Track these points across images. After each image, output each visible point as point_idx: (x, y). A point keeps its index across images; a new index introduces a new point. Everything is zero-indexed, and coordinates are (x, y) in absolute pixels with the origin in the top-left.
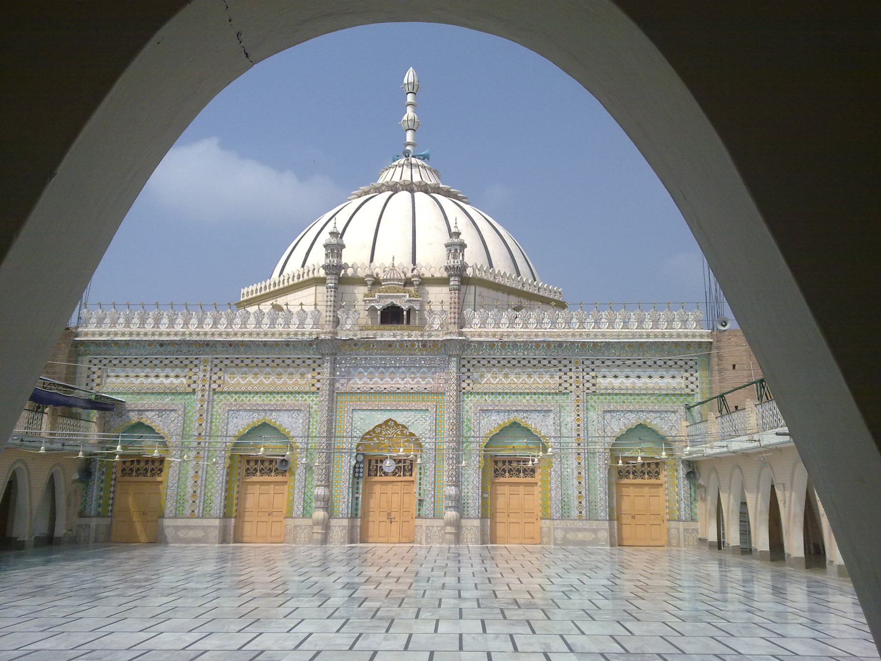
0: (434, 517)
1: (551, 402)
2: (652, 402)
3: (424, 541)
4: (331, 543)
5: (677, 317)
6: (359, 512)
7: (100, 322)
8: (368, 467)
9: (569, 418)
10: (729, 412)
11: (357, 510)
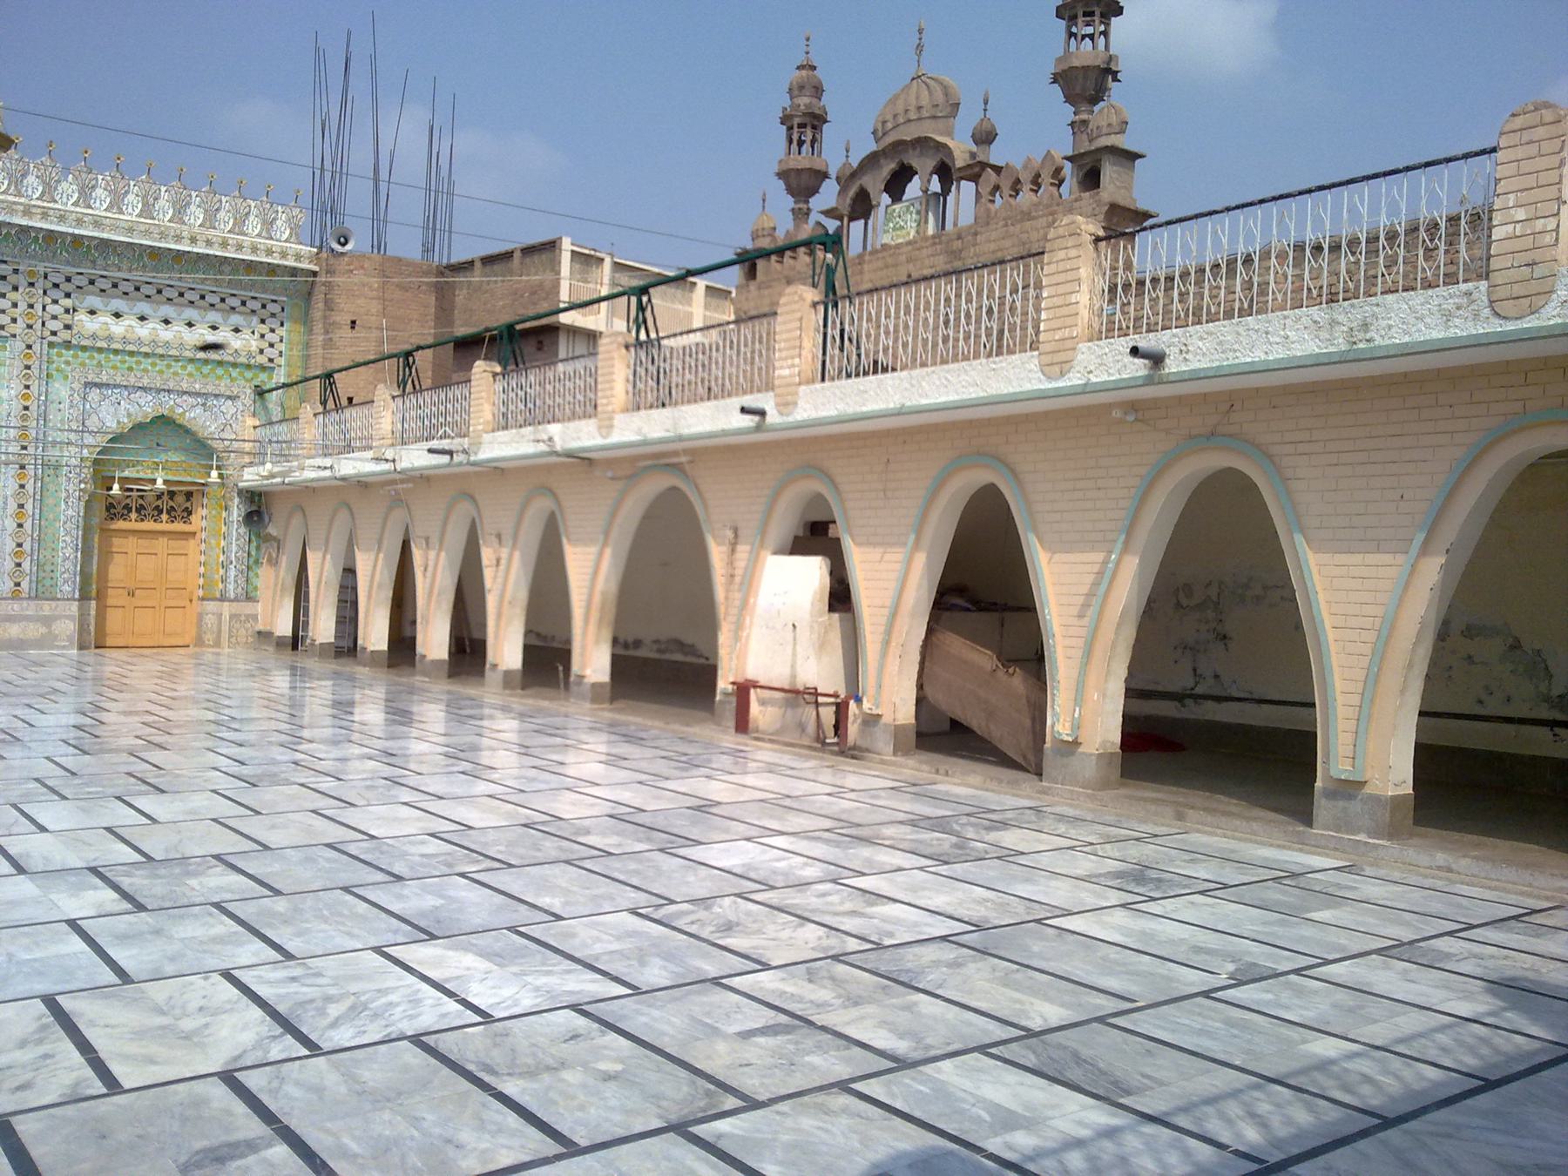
2: (190, 375)
5: (254, 211)
10: (338, 408)
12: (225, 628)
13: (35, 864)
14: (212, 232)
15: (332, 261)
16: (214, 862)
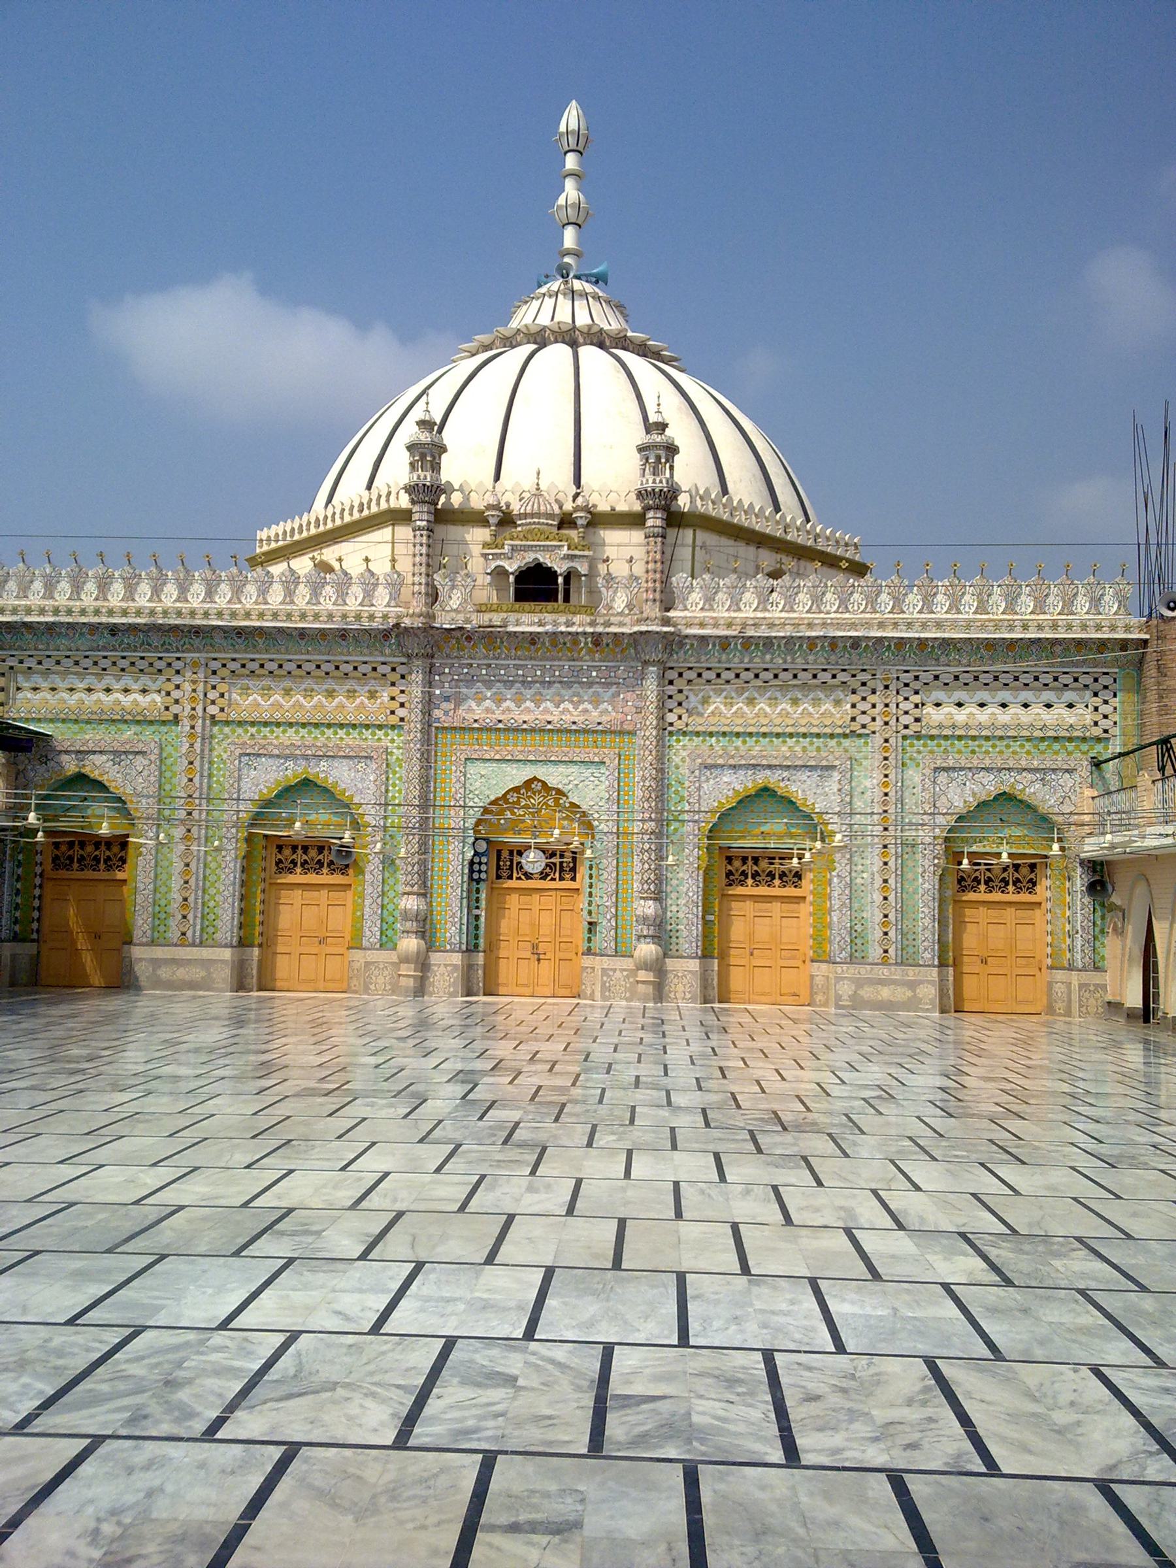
0: (617, 953)
1: (833, 752)
2: (1028, 753)
3: (598, 994)
8: (494, 864)
9: (869, 781)
11: (477, 937)
12: (1075, 997)
13: (911, 1222)
14: (1042, 617)
16: (1077, 1245)
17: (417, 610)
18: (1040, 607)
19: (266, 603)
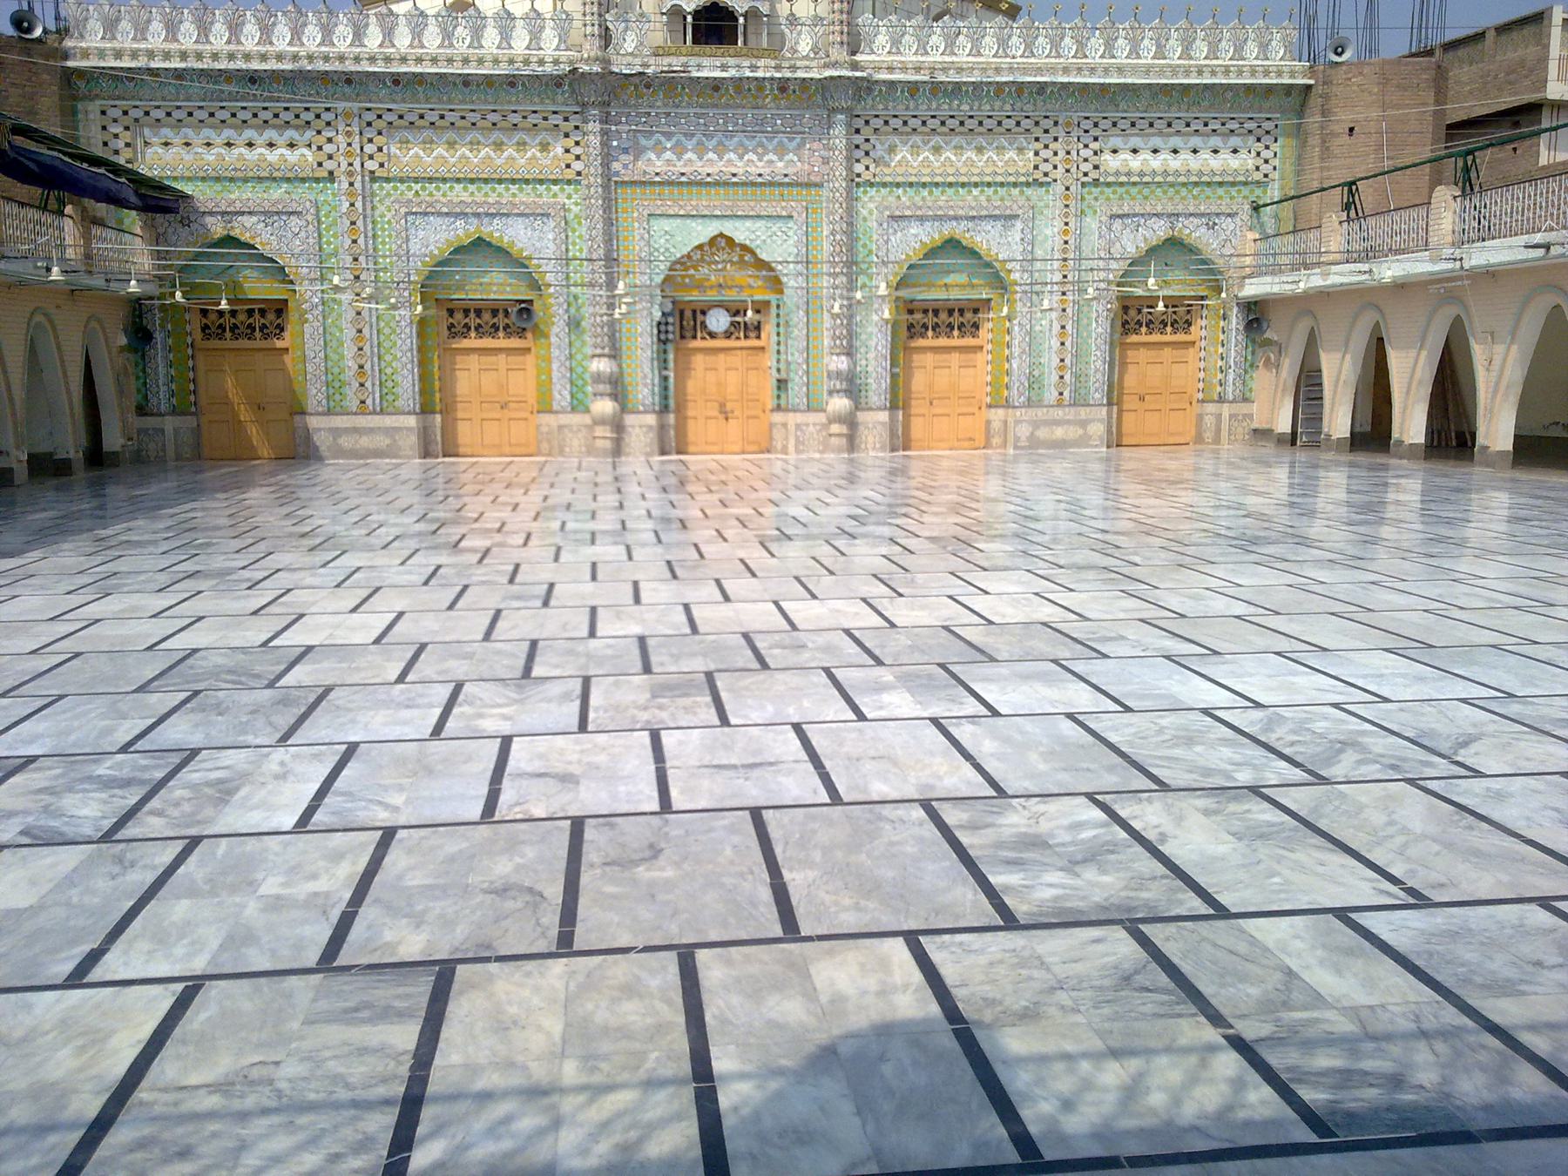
0: (809, 409)
1: (1015, 200)
3: (791, 448)
4: (628, 454)
6: (672, 402)
7: (111, 26)
8: (682, 324)
9: (1050, 232)
11: (666, 398)
14: (1215, 62)
15: (1329, 71)
17: (592, 54)
18: (1213, 53)
19: (423, 47)
